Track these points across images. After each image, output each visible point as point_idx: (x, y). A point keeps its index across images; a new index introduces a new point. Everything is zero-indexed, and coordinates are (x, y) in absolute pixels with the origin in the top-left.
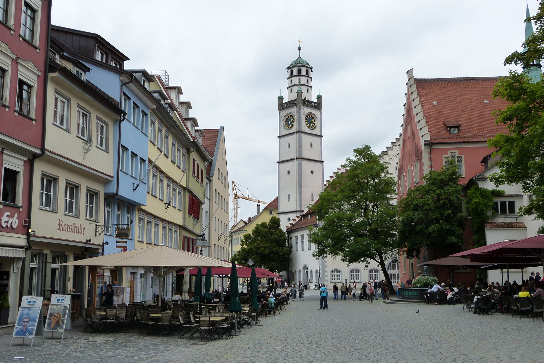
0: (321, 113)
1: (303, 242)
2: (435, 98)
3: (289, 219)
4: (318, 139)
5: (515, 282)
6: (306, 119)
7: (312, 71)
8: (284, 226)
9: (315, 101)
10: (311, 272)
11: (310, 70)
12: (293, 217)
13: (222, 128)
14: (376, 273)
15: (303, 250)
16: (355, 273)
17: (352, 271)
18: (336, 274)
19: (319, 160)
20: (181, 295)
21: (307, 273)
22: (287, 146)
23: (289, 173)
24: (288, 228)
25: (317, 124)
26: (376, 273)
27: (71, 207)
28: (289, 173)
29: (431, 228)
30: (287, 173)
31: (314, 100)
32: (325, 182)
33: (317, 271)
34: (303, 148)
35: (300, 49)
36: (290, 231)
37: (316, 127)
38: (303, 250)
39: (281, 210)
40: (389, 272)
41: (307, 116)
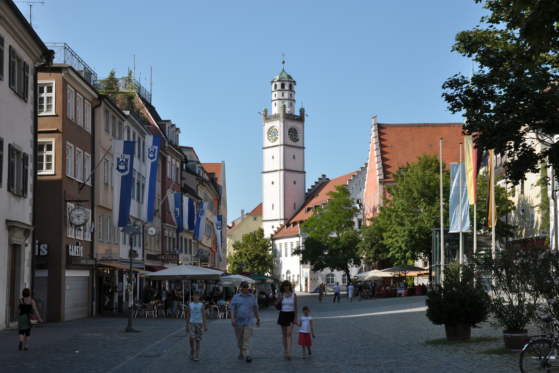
1: (286, 249)
3: (273, 227)
4: (300, 151)
6: (289, 132)
8: (267, 235)
10: (294, 276)
11: (293, 84)
12: (277, 225)
13: (223, 162)
15: (286, 256)
18: (330, 277)
19: (302, 170)
21: (93, 220)
23: (273, 183)
24: (272, 236)
25: (300, 136)
27: (186, 253)
28: (273, 183)
30: (271, 183)
31: (297, 113)
32: (307, 191)
33: (298, 276)
34: (311, 350)
35: (283, 55)
36: (273, 238)
37: (298, 140)
38: (286, 256)
39: (265, 217)
41: (290, 130)
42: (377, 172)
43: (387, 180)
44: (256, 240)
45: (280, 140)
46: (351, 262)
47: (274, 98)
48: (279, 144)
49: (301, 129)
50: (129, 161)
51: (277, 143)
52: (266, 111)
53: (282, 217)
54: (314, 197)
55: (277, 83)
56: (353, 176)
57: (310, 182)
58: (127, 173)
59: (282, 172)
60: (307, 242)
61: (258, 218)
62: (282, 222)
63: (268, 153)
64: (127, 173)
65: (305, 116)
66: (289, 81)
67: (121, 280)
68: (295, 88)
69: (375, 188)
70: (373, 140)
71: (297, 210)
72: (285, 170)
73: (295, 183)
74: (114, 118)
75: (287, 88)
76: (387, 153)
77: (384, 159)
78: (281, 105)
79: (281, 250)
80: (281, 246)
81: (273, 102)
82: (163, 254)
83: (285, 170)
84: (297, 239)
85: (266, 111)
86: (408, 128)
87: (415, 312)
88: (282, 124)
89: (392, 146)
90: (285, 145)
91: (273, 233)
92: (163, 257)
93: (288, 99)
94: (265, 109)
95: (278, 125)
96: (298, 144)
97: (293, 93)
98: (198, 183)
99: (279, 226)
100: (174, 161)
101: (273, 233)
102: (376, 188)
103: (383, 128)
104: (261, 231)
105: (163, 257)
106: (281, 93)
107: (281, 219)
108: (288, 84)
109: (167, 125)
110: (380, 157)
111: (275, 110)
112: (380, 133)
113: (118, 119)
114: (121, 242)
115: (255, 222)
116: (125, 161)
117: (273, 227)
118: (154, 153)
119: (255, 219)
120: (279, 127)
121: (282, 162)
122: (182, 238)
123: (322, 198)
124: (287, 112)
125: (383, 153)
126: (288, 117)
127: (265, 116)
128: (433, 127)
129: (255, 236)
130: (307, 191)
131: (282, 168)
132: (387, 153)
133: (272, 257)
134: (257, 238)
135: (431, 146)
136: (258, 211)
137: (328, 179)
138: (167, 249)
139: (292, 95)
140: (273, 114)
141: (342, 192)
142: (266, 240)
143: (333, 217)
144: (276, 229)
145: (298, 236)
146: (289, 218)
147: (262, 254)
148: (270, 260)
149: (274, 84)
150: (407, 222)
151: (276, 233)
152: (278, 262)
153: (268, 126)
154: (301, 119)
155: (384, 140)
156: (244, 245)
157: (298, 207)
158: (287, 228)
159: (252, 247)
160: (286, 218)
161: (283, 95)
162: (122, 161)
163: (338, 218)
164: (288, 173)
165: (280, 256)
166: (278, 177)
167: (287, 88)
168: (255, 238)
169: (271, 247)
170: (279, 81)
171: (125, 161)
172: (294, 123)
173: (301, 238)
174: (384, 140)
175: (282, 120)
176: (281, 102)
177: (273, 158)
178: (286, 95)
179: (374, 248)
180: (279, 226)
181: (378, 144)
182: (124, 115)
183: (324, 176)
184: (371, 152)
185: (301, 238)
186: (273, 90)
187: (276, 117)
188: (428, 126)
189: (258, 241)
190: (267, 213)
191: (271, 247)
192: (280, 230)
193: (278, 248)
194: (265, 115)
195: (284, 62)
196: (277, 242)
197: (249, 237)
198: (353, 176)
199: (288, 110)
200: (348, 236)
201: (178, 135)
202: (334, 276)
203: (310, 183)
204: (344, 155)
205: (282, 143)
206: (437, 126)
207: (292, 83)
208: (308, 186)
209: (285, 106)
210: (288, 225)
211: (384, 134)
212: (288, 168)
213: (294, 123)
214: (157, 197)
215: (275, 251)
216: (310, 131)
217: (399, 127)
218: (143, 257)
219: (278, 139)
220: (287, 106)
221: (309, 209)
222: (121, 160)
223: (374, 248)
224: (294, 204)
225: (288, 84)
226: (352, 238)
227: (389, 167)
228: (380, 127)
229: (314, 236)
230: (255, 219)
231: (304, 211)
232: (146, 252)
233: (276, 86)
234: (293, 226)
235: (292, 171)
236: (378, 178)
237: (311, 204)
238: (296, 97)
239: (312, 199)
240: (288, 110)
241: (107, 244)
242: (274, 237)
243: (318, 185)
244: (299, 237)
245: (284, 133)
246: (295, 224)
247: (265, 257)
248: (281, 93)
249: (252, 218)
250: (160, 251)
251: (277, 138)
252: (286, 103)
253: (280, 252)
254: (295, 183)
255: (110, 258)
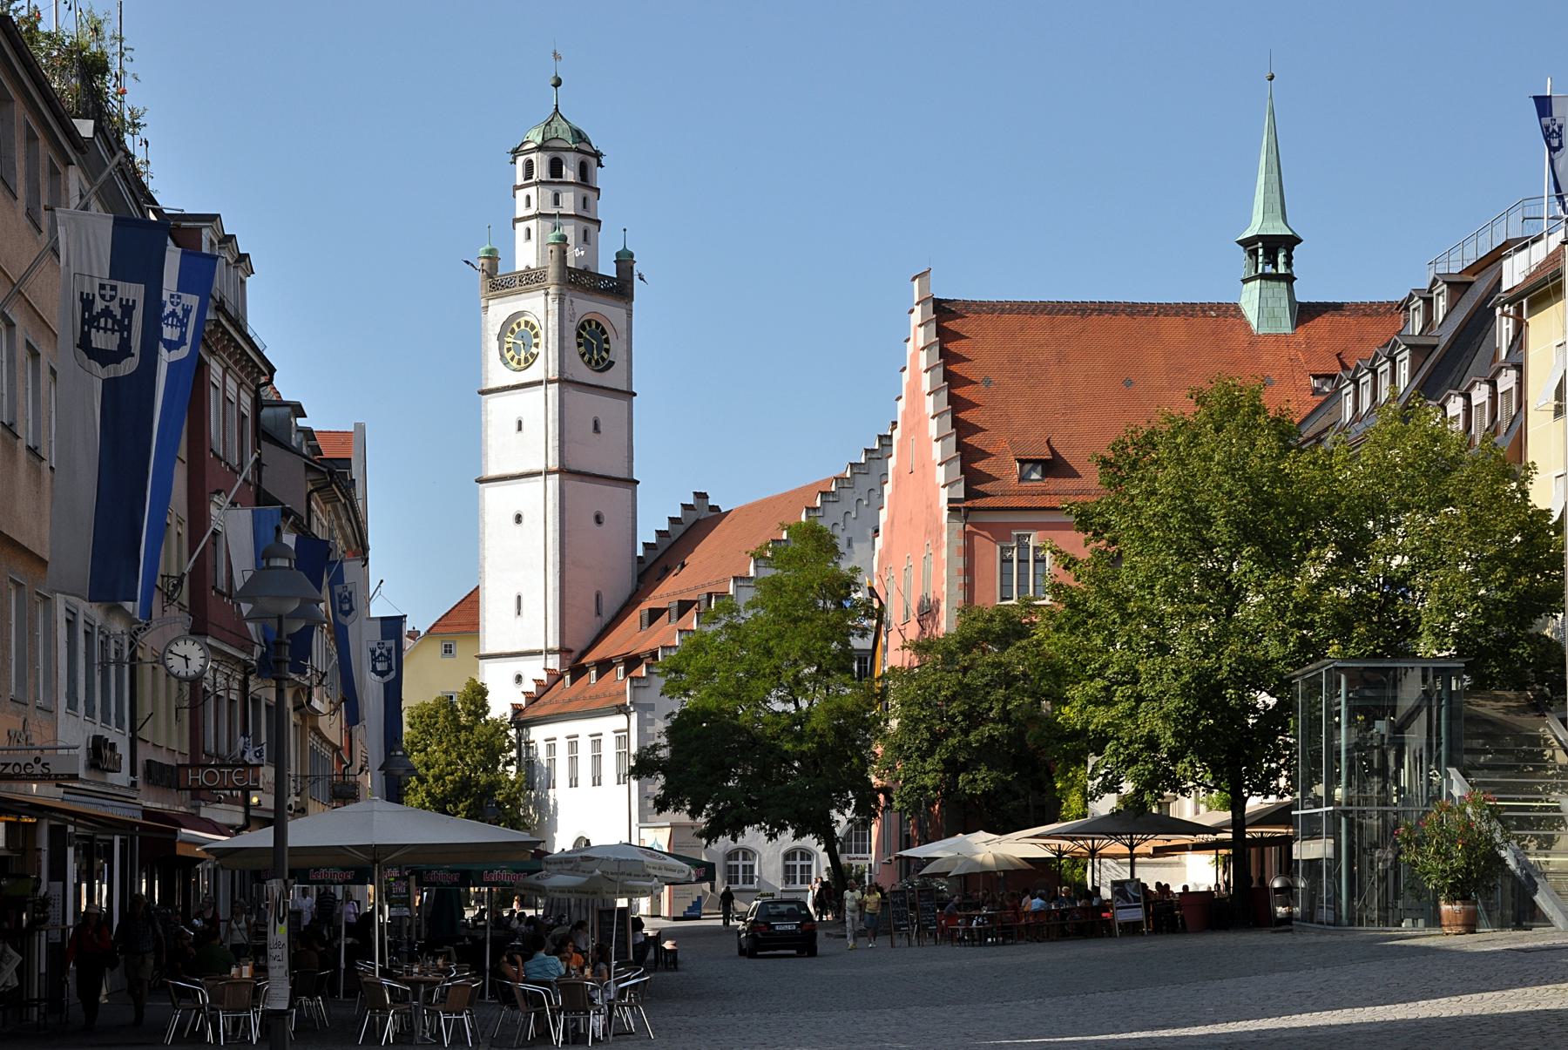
0: (630, 315)
2: (583, 843)
3: (519, 679)
5: (1158, 884)
6: (579, 335)
7: (600, 165)
8: (499, 706)
9: (611, 272)
11: (593, 161)
12: (535, 670)
13: (360, 428)
14: (806, 863)
15: (574, 782)
16: (798, 863)
17: (789, 855)
18: (741, 863)
19: (625, 475)
20: (734, 839)
22: (515, 426)
23: (519, 519)
24: (517, 710)
25: (616, 350)
26: (806, 863)
28: (519, 519)
29: (1394, 563)
30: (525, 519)
31: (608, 268)
32: (640, 553)
36: (521, 719)
37: (611, 364)
38: (574, 782)
39: (488, 646)
40: (844, 859)
41: (583, 327)
42: (940, 475)
43: (978, 503)
44: (460, 728)
45: (545, 365)
46: (848, 804)
47: (521, 211)
48: (541, 376)
49: (621, 325)
50: (138, 315)
51: (536, 372)
52: (492, 257)
53: (554, 643)
54: (666, 571)
55: (533, 156)
56: (823, 493)
57: (653, 516)
58: (129, 366)
59: (554, 480)
60: (680, 729)
61: (460, 648)
62: (554, 662)
63: (499, 410)
64: (129, 366)
65: (636, 278)
66: (578, 151)
67: (58, 873)
68: (600, 177)
69: (928, 533)
70: (915, 357)
71: (607, 617)
72: (564, 471)
73: (598, 519)
74: (31, 138)
75: (569, 174)
76: (972, 405)
77: (962, 429)
78: (551, 237)
79: (552, 761)
80: (551, 748)
81: (521, 227)
82: (196, 765)
83: (564, 471)
84: (620, 721)
85: (492, 257)
86: (1043, 318)
87: (1514, 1017)
88: (554, 306)
89: (988, 382)
90: (563, 381)
91: (522, 700)
92: (201, 777)
93: (576, 216)
94: (490, 251)
95: (539, 307)
96: (610, 379)
97: (591, 195)
98: (310, 487)
99: (543, 676)
100: (232, 385)
101: (522, 700)
102: (933, 531)
103: (954, 315)
104: (478, 695)
105: (201, 777)
106: (548, 193)
107: (549, 652)
108: (572, 161)
109: (206, 234)
110: (948, 418)
111: (526, 254)
112: (944, 335)
113: (44, 149)
114: (63, 701)
115: (448, 660)
116: (118, 313)
117: (519, 679)
118: (183, 324)
119: (448, 650)
120: (542, 317)
121: (553, 443)
122: (256, 702)
123: (708, 569)
124: (571, 264)
125: (957, 404)
126: (576, 280)
127: (489, 276)
128: (1131, 314)
129: (454, 710)
130: (640, 553)
131: (554, 464)
132: (972, 405)
133: (520, 790)
134: (463, 720)
135: (1129, 383)
136: (463, 620)
137: (715, 508)
138: (210, 745)
139: (590, 203)
140: (520, 267)
141: (812, 544)
142: (498, 728)
143: (780, 636)
144: (532, 688)
145: (622, 710)
146: (578, 647)
147: (483, 778)
148: (513, 800)
149: (521, 160)
150: (1182, 647)
151: (532, 699)
152: (541, 805)
153: (499, 310)
154: (620, 288)
155: (959, 359)
156: (414, 744)
157: (608, 612)
158: (573, 682)
159: (446, 752)
160: (568, 645)
161: (557, 203)
162: (107, 312)
163: (798, 643)
164: (574, 484)
165: (550, 783)
166: (538, 500)
167: (569, 174)
168: (456, 718)
169: (513, 754)
170: (540, 148)
171: (118, 313)
172: (597, 297)
173: (634, 717)
174: (959, 359)
175: (552, 290)
176: (548, 224)
177: (521, 426)
178: (569, 201)
179: (941, 753)
180: (543, 676)
181: (940, 370)
182: (72, 133)
183: (701, 496)
184: (910, 403)
185: (634, 717)
186: (520, 180)
187: (530, 279)
188: (1115, 313)
189: (470, 729)
190: (498, 628)
191: (513, 754)
192: (544, 688)
193: (542, 755)
194: (491, 273)
195: (558, 83)
196: (538, 734)
197: (434, 715)
198: (823, 493)
199: (574, 254)
200: (840, 708)
201: (243, 282)
202: (809, 858)
203: (652, 522)
204: (725, 440)
205: (553, 373)
206: (1146, 313)
207: (589, 159)
208: (646, 534)
209: (563, 239)
210: (578, 671)
211: (958, 336)
212: (574, 467)
213: (597, 297)
214: (175, 528)
215: (528, 765)
216: (652, 332)
217: (1011, 311)
218: (133, 773)
219: (540, 360)
220: (571, 240)
221: (654, 615)
222: (99, 305)
223: (941, 753)
224: (598, 596)
225: (572, 161)
226: (852, 714)
227: (984, 455)
228: (943, 312)
229: (712, 704)
230: (448, 650)
231: (634, 618)
232: (144, 754)
233: (529, 166)
234: (599, 676)
235: (589, 475)
236: (944, 495)
237: (666, 593)
238: (602, 209)
239: (660, 579)
240: (574, 254)
241: (12, 707)
242: (524, 717)
243: (681, 529)
244: (628, 714)
245: (561, 339)
246: (604, 666)
247: (493, 786)
248: (548, 193)
249: (436, 648)
250: (186, 750)
251: (534, 356)
252: (569, 230)
253: (550, 771)
254: (598, 519)
255: (38, 769)
